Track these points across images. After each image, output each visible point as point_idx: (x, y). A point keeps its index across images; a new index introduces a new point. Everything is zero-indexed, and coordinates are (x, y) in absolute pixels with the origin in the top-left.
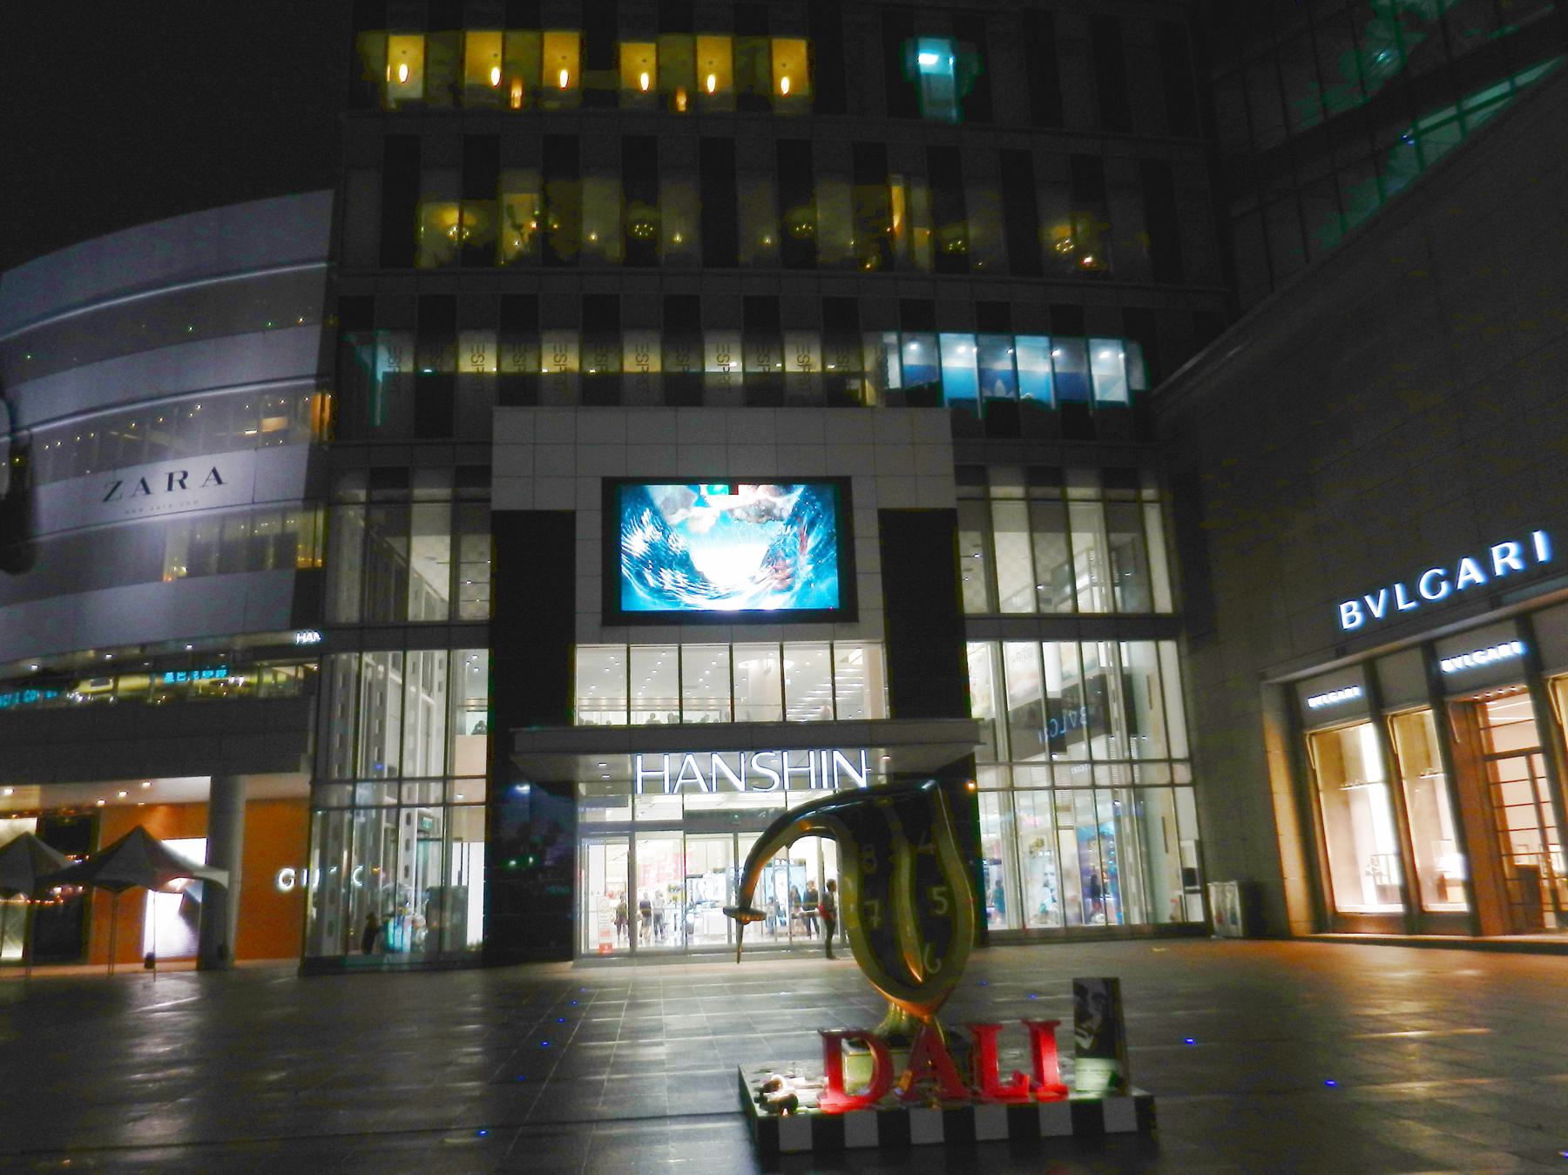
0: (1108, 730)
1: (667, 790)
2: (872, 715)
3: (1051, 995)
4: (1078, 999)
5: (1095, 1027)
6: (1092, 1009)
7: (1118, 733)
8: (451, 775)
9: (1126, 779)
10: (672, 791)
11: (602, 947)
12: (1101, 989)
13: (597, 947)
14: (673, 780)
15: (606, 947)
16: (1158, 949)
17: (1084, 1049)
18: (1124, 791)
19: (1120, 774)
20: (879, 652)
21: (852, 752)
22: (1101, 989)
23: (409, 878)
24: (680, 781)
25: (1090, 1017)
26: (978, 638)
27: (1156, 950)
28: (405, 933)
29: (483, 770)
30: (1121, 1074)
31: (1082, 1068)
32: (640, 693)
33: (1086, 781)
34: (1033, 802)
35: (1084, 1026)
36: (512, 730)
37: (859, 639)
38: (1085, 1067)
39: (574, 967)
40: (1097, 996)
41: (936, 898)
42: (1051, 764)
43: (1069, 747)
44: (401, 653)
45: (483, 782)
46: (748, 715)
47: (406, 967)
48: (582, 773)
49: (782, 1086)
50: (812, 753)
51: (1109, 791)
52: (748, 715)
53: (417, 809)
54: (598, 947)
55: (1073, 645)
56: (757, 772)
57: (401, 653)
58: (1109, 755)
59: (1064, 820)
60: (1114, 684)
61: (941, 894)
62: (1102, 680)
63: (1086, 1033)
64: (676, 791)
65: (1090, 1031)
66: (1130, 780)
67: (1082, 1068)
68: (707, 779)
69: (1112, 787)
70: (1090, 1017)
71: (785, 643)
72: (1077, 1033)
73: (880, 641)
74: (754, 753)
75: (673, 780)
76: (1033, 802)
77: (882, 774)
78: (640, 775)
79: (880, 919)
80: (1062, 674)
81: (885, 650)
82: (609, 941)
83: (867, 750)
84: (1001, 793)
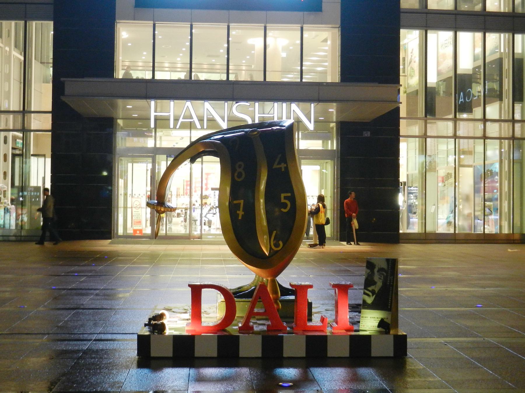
0: (501, 99)
1: (172, 126)
2: (332, 79)
3: (411, 274)
4: (368, 271)
5: (377, 290)
6: (376, 278)
7: (506, 100)
8: (29, 110)
9: (509, 133)
10: (175, 127)
11: (135, 231)
12: (384, 265)
13: (132, 232)
14: (176, 120)
15: (138, 232)
16: (511, 250)
17: (368, 304)
18: (507, 141)
19: (506, 129)
20: (337, 33)
21: (306, 105)
22: (384, 265)
23: (7, 179)
24: (181, 120)
25: (374, 283)
26: (412, 26)
27: (509, 250)
28: (11, 218)
29: (50, 109)
30: (389, 321)
31: (365, 316)
32: (244, 61)
33: (480, 134)
34: (447, 148)
35: (370, 289)
36: (62, 79)
37: (322, 24)
38: (366, 316)
39: (110, 243)
40: (381, 270)
41: (283, 200)
42: (455, 120)
43: (474, 109)
44: (22, 23)
45: (50, 116)
46: (251, 76)
47: (13, 238)
48: (121, 113)
49: (166, 318)
50: (276, 104)
51: (498, 141)
52: (251, 76)
53: (11, 133)
54: (132, 232)
55: (479, 35)
56: (238, 117)
57: (22, 23)
58: (500, 116)
59: (466, 159)
60: (507, 65)
61: (285, 198)
62: (500, 62)
63: (370, 294)
64: (178, 127)
65: (373, 292)
66: (511, 134)
67: (365, 316)
68: (201, 120)
69: (500, 138)
70: (374, 283)
71: (304, 25)
72: (365, 293)
73: (338, 26)
74: (234, 102)
75: (176, 120)
76: (447, 148)
77: (333, 122)
78: (153, 114)
79: (243, 213)
80: (474, 56)
81: (340, 33)
82: (140, 228)
83: (316, 104)
84: (421, 139)
